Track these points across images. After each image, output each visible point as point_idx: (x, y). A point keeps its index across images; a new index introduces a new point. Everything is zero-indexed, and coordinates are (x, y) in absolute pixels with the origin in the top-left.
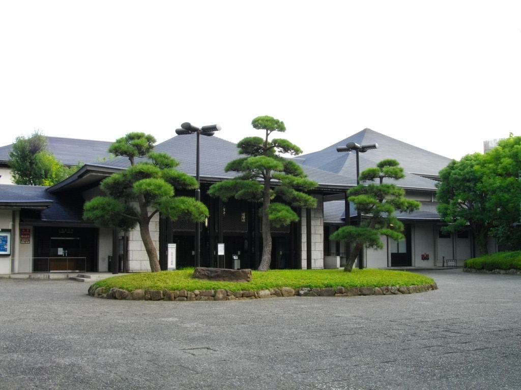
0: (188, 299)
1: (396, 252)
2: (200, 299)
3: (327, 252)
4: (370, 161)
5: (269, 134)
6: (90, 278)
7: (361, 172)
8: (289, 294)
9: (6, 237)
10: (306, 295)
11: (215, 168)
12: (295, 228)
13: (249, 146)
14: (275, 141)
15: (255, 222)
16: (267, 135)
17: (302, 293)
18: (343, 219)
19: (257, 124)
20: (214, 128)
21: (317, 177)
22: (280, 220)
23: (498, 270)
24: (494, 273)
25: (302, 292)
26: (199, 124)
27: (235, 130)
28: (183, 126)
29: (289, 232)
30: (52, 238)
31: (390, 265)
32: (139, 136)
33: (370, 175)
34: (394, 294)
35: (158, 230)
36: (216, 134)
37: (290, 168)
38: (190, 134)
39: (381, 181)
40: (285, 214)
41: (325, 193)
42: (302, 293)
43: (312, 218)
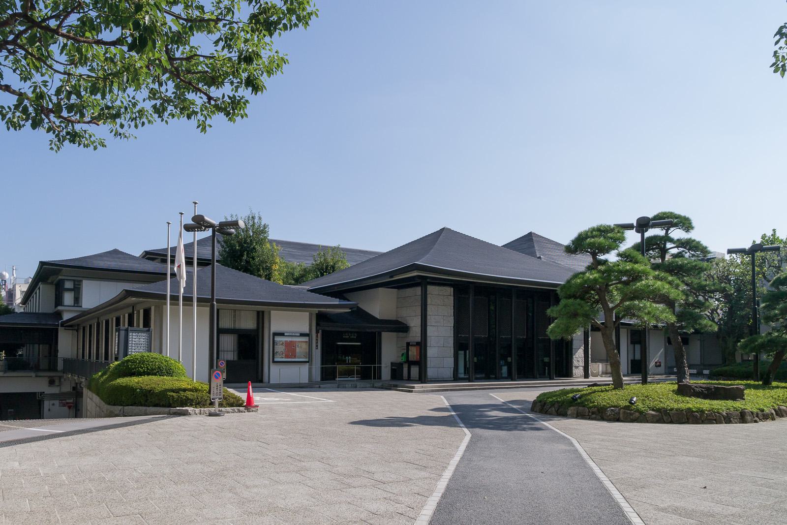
29: (487, 336)
31: (630, 372)
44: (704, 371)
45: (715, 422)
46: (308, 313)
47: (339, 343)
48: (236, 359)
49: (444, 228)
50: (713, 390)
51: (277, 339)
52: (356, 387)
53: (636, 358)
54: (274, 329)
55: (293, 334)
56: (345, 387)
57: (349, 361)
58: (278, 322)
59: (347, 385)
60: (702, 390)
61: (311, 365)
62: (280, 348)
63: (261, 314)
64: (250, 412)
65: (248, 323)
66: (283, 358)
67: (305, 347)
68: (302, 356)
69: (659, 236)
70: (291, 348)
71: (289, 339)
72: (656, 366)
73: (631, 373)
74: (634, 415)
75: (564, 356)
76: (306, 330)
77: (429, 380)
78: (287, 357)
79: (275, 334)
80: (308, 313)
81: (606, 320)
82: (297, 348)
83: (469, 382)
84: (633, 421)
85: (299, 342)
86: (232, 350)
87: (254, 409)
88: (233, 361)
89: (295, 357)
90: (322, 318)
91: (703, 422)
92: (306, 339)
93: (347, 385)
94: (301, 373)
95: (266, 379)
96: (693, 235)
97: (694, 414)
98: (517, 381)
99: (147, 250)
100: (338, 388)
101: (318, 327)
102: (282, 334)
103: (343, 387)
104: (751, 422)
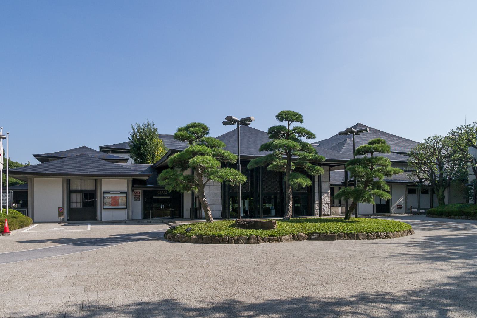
0: (229, 243)
1: (379, 204)
2: (238, 243)
3: (332, 204)
4: (363, 141)
5: (290, 124)
6: (175, 223)
7: (356, 149)
8: (303, 238)
9: (248, 190)
10: (316, 239)
11: (253, 151)
12: (311, 189)
13: (275, 132)
14: (295, 129)
15: (282, 186)
16: (289, 125)
17: (313, 238)
18: (342, 183)
19: (281, 117)
20: (249, 119)
21: (325, 155)
22: (376, 183)
23: (453, 216)
24: (450, 218)
25: (313, 237)
26: (237, 117)
27: (263, 123)
28: (227, 118)
29: (306, 192)
30: (154, 197)
31: (375, 212)
32: (194, 126)
33: (365, 151)
34: (383, 238)
35: (221, 191)
36: (252, 125)
37: (305, 147)
38: (233, 124)
39: (372, 155)
40: (304, 182)
41: (331, 165)
42: (313, 238)
43: (322, 182)
44: (421, 210)
45: (227, 243)
46: (127, 180)
47: (169, 197)
48: (81, 207)
49: (358, 124)
50: (253, 223)
51: (106, 195)
52: (150, 222)
53: (381, 204)
54: (104, 189)
55: (116, 192)
56: (143, 223)
57: (162, 207)
58: (107, 185)
59: (144, 222)
60: (245, 223)
61: (129, 209)
62: (108, 200)
63: (68, 180)
64: (4, 235)
65: (89, 186)
66: (110, 206)
67: (124, 199)
68: (123, 205)
69: (275, 126)
70: (115, 201)
71: (114, 195)
72: (397, 208)
73: (376, 213)
74: (185, 238)
75: (195, 202)
76: (125, 189)
77: (203, 218)
78: (112, 205)
79: (105, 193)
80: (127, 180)
81: (345, 181)
82: (119, 200)
83: (260, 218)
84: (185, 242)
85: (120, 196)
86: (80, 202)
87: (7, 234)
88: (80, 208)
89: (118, 205)
90: (136, 182)
91: (220, 243)
92: (125, 195)
93: (144, 222)
94: (123, 215)
95: (99, 218)
96: (304, 125)
97: (216, 238)
98: (194, 220)
99: (101, 146)
100: (138, 223)
101: (133, 188)
102: (109, 193)
103: (142, 223)
104: (254, 243)
